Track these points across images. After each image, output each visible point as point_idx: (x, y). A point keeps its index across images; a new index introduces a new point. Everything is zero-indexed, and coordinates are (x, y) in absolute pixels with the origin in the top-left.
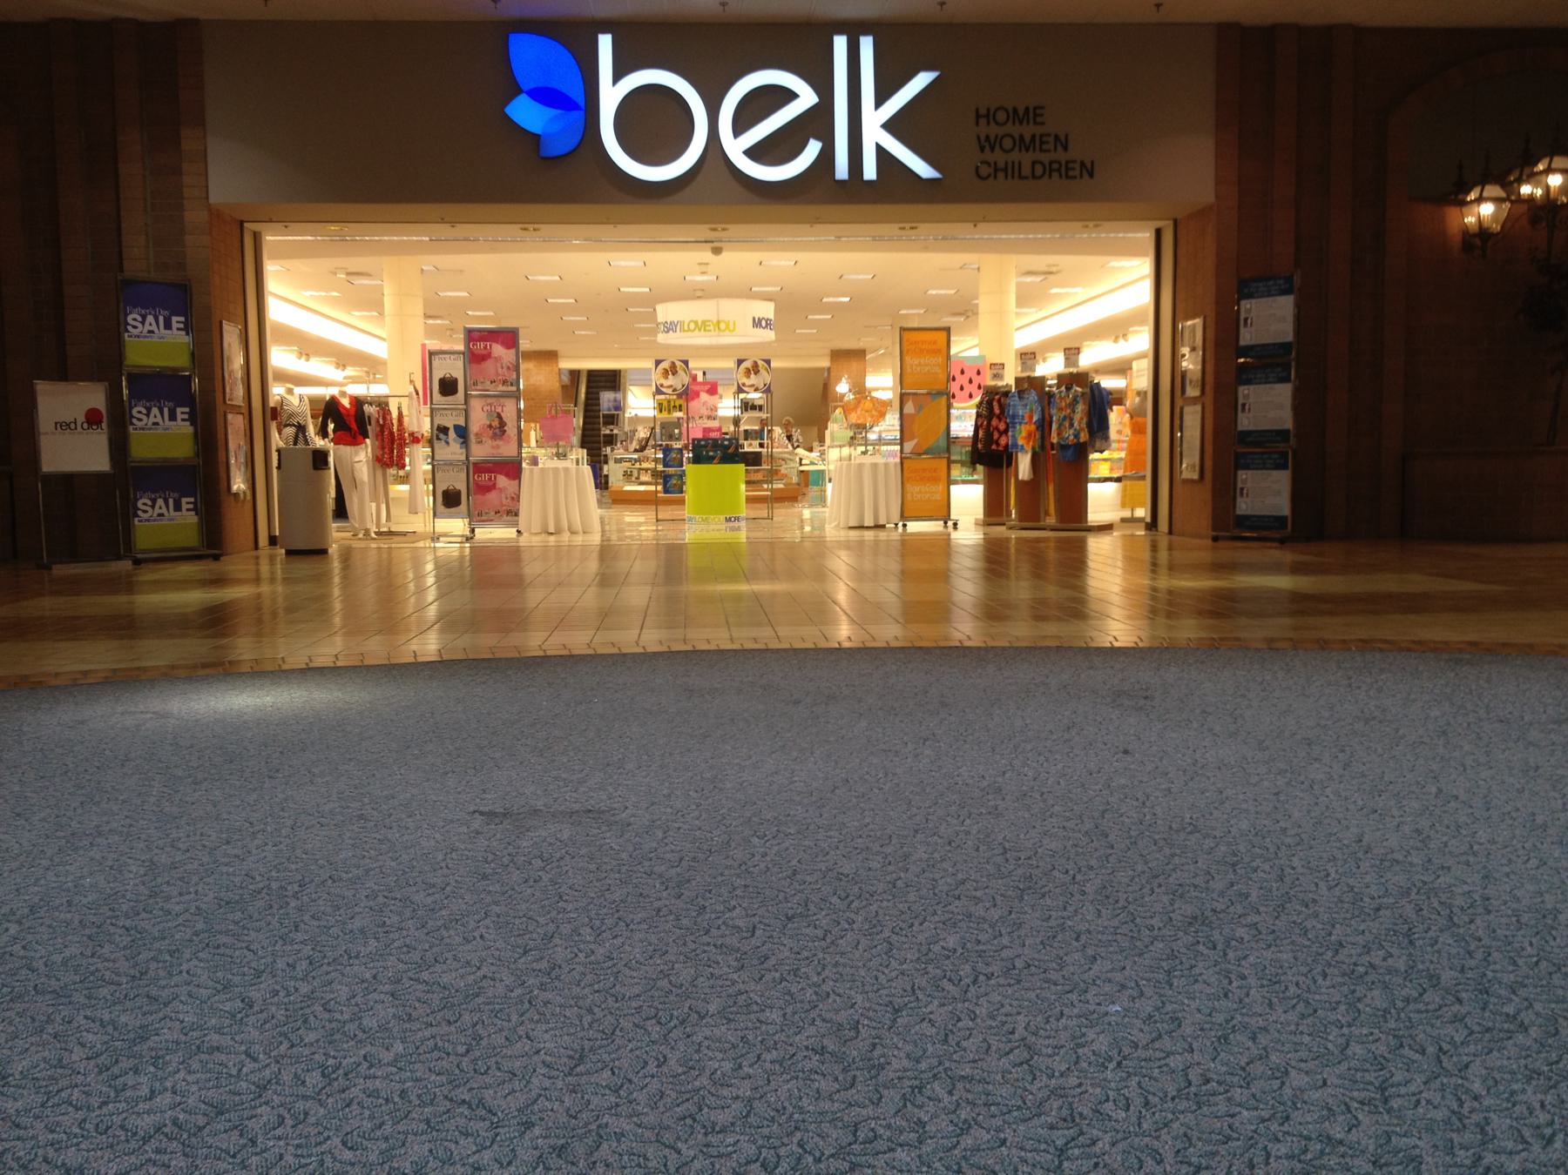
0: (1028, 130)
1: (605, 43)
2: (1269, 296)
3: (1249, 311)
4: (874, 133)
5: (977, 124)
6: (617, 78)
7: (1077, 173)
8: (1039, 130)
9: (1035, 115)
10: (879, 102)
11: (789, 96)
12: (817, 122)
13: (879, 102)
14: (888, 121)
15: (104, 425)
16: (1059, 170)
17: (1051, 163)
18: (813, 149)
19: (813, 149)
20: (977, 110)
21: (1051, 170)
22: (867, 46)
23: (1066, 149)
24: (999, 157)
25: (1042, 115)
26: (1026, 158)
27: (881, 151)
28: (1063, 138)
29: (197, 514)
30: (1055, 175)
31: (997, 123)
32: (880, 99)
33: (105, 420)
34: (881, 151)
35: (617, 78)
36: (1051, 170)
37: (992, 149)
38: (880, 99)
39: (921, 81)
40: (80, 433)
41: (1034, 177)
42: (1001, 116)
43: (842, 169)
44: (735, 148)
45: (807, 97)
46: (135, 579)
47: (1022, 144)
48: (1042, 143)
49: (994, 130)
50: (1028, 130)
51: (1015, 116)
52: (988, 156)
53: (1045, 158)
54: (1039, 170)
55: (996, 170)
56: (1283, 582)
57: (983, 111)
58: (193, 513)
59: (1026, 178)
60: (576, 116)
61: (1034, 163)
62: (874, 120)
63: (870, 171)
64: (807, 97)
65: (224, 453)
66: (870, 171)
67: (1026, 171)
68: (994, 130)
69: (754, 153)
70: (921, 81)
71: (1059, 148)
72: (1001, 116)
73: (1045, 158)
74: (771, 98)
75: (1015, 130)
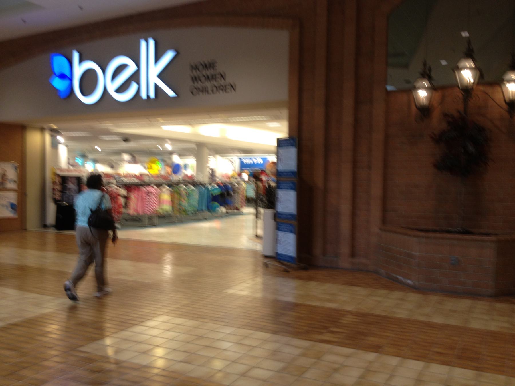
0: (209, 72)
1: (171, 93)
4: (155, 80)
12: (135, 77)
18: (134, 87)
24: (199, 85)
26: (208, 84)
43: (144, 95)
44: (111, 91)
45: (132, 68)
46: (224, 291)
47: (208, 78)
50: (209, 72)
51: (205, 66)
56: (39, 230)
64: (132, 68)
66: (152, 95)
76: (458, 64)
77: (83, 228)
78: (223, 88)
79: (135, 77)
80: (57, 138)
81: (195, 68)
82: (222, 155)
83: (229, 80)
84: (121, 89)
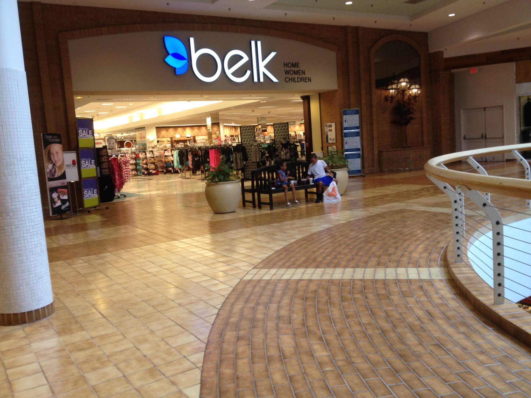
0: (296, 69)
1: (275, 80)
2: (352, 114)
3: (346, 118)
4: (262, 69)
5: (284, 67)
6: (196, 51)
7: (307, 81)
8: (298, 69)
9: (297, 65)
10: (263, 60)
11: (241, 58)
12: (249, 65)
13: (263, 60)
14: (266, 65)
15: (76, 165)
16: (303, 80)
17: (302, 78)
18: (249, 72)
19: (249, 72)
20: (284, 63)
21: (302, 80)
22: (259, 43)
23: (304, 74)
24: (290, 76)
25: (299, 65)
26: (296, 76)
27: (264, 74)
28: (304, 71)
29: (98, 194)
30: (303, 81)
31: (289, 67)
32: (263, 59)
33: (76, 163)
34: (264, 74)
35: (196, 51)
36: (302, 80)
37: (288, 74)
38: (263, 59)
39: (273, 54)
40: (71, 168)
41: (298, 82)
42: (290, 65)
43: (256, 80)
44: (229, 72)
45: (246, 59)
48: (299, 72)
49: (288, 69)
50: (296, 69)
52: (287, 76)
53: (300, 76)
54: (299, 80)
55: (290, 80)
57: (285, 64)
58: (96, 194)
59: (296, 82)
60: (184, 62)
61: (298, 78)
62: (262, 64)
63: (262, 80)
64: (246, 59)
65: (364, 144)
66: (262, 80)
67: (296, 80)
68: (288, 69)
69: (234, 74)
70: (273, 54)
71: (303, 74)
72: (290, 65)
73: (300, 76)
74: (236, 59)
75: (293, 69)
76: (74, 96)
77: (402, 86)
78: (302, 80)
79: (249, 65)
80: (413, 85)
81: (286, 65)
82: (118, 182)
83: (307, 75)
84: (237, 74)
